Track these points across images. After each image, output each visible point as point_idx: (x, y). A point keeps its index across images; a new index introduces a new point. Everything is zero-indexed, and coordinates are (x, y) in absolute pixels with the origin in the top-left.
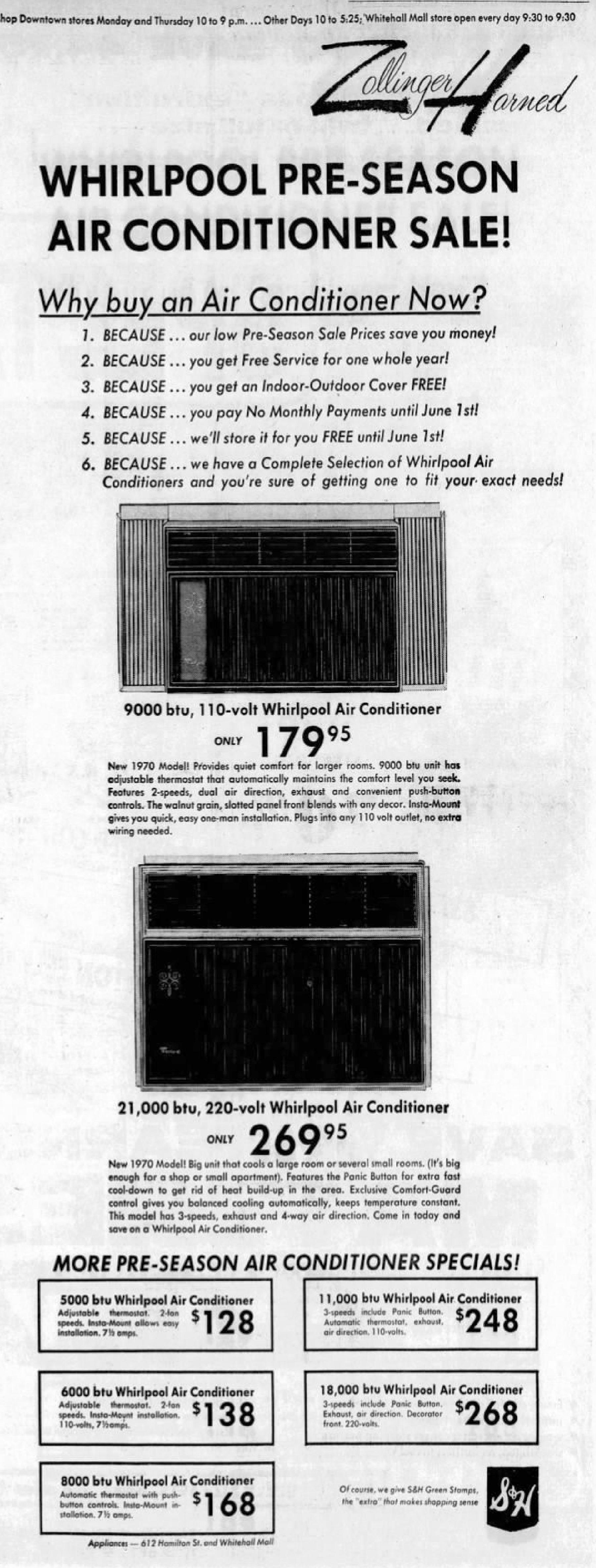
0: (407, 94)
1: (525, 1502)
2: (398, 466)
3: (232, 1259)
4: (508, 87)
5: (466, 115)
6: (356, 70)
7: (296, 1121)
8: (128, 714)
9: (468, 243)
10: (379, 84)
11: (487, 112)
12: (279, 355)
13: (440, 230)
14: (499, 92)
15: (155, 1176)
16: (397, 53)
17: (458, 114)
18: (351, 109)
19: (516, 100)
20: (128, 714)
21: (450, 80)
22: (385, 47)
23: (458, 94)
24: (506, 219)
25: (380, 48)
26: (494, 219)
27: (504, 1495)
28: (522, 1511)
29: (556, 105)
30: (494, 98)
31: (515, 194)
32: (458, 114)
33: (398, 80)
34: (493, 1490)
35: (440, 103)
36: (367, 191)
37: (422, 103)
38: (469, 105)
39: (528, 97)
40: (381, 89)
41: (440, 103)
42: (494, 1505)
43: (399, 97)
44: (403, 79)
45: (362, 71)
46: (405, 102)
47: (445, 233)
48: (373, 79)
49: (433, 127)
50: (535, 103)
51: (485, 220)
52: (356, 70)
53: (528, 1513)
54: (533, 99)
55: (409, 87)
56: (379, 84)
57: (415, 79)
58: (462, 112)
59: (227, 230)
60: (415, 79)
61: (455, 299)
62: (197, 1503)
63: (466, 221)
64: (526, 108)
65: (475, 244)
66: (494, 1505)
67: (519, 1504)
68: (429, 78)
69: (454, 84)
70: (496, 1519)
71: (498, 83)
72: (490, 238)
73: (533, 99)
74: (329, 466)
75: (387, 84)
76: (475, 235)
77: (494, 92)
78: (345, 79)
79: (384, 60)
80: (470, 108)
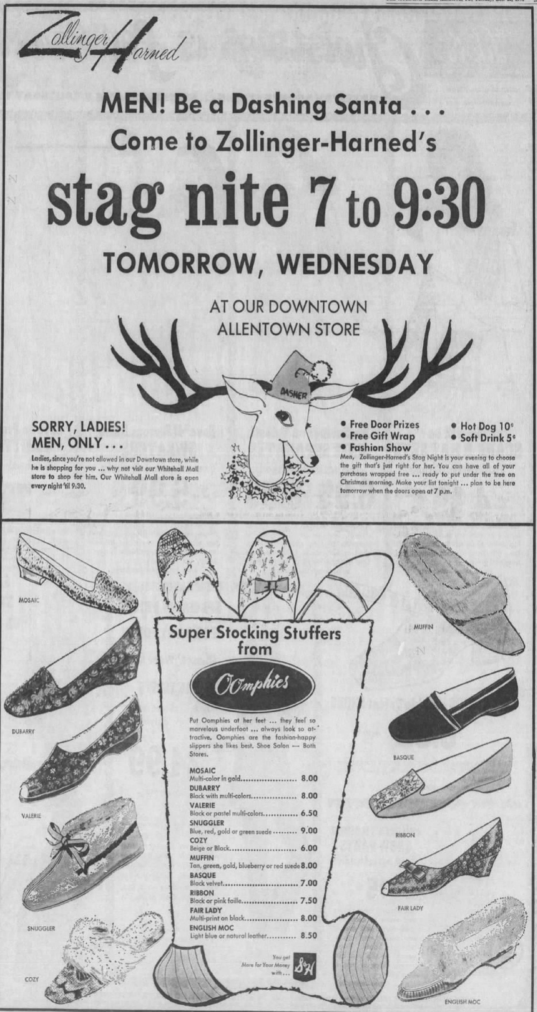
0: (79, 45)
1: (310, 969)
4: (142, 44)
5: (115, 61)
6: (48, 29)
10: (63, 39)
11: (129, 59)
14: (138, 47)
15: (271, 866)
16: (74, 19)
17: (111, 60)
18: (43, 54)
19: (148, 52)
21: (107, 38)
22: (67, 15)
23: (111, 47)
27: (301, 965)
28: (309, 972)
29: (173, 56)
30: (134, 51)
32: (111, 60)
34: (296, 964)
35: (101, 53)
37: (89, 53)
38: (118, 54)
39: (155, 51)
41: (101, 53)
43: (74, 47)
44: (78, 35)
45: (52, 30)
46: (78, 51)
48: (58, 36)
49: (95, 68)
50: (159, 55)
52: (48, 29)
53: (311, 974)
54: (159, 52)
55: (81, 42)
56: (63, 39)
57: (85, 36)
58: (113, 59)
59: (324, 262)
60: (85, 36)
64: (154, 57)
66: (296, 970)
67: (307, 970)
68: (93, 37)
69: (109, 41)
71: (136, 41)
73: (159, 52)
75: (67, 39)
77: (134, 46)
78: (40, 35)
79: (66, 23)
80: (119, 56)
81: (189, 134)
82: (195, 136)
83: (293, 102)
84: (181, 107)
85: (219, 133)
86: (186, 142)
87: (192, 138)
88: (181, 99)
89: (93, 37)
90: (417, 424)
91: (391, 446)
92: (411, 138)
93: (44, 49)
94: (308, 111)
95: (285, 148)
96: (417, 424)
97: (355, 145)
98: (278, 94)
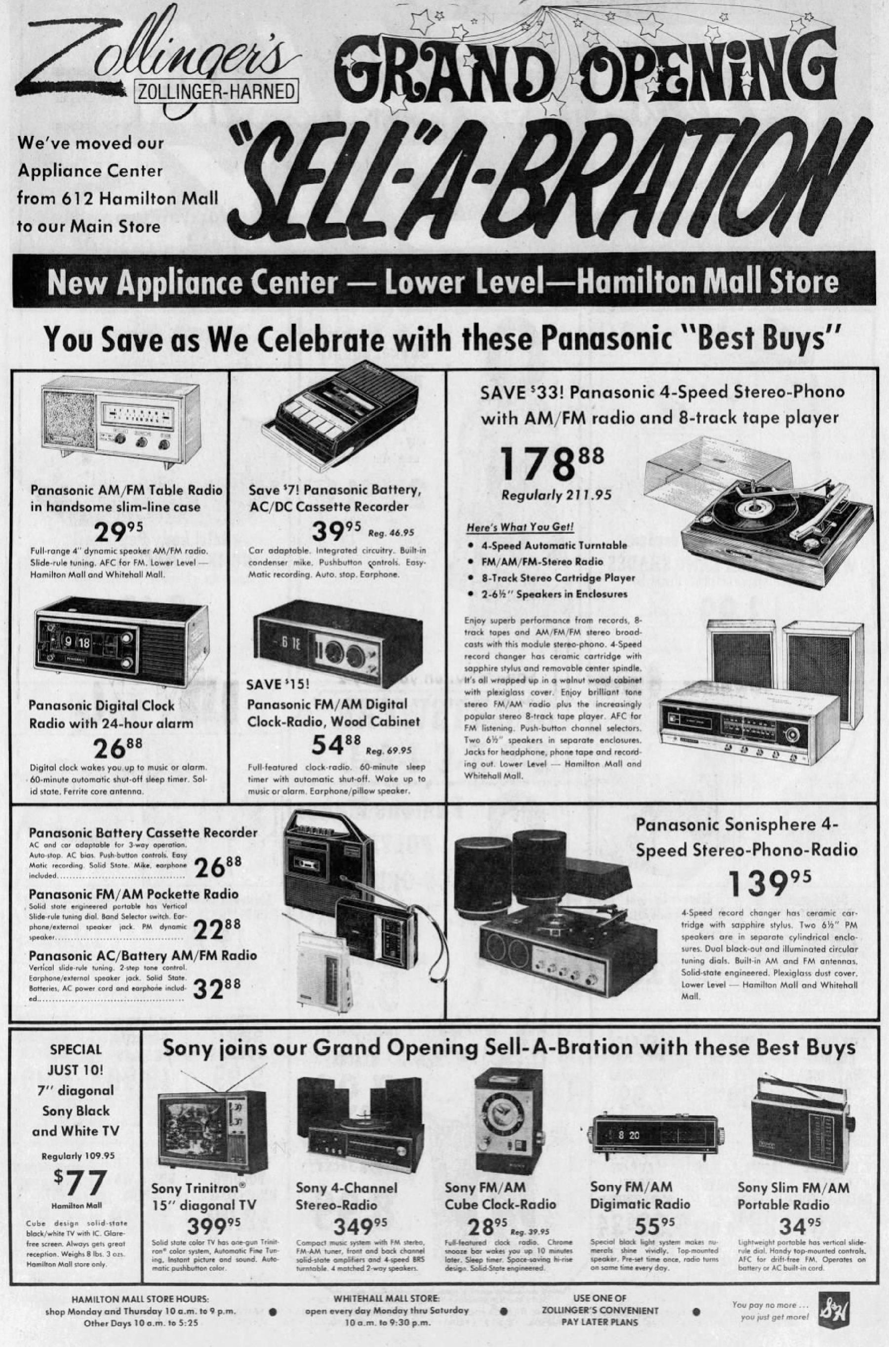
2: (75, 1073)
12: (111, 328)
22: (99, 26)
25: (93, 26)
27: (828, 1308)
33: (162, 52)
34: (822, 1305)
36: (680, 397)
40: (129, 68)
42: (823, 1312)
44: (171, 51)
46: (120, 84)
53: (843, 1319)
56: (128, 58)
61: (400, 338)
62: (58, 1181)
66: (822, 1315)
67: (838, 1313)
68: (218, 51)
74: (488, 1053)
75: (142, 59)
83: (100, 226)
84: (763, 1050)
86: (17, 227)
88: (762, 1043)
89: (218, 51)
93: (59, 83)
94: (461, 1053)
95: (468, 1052)
98: (781, 818)
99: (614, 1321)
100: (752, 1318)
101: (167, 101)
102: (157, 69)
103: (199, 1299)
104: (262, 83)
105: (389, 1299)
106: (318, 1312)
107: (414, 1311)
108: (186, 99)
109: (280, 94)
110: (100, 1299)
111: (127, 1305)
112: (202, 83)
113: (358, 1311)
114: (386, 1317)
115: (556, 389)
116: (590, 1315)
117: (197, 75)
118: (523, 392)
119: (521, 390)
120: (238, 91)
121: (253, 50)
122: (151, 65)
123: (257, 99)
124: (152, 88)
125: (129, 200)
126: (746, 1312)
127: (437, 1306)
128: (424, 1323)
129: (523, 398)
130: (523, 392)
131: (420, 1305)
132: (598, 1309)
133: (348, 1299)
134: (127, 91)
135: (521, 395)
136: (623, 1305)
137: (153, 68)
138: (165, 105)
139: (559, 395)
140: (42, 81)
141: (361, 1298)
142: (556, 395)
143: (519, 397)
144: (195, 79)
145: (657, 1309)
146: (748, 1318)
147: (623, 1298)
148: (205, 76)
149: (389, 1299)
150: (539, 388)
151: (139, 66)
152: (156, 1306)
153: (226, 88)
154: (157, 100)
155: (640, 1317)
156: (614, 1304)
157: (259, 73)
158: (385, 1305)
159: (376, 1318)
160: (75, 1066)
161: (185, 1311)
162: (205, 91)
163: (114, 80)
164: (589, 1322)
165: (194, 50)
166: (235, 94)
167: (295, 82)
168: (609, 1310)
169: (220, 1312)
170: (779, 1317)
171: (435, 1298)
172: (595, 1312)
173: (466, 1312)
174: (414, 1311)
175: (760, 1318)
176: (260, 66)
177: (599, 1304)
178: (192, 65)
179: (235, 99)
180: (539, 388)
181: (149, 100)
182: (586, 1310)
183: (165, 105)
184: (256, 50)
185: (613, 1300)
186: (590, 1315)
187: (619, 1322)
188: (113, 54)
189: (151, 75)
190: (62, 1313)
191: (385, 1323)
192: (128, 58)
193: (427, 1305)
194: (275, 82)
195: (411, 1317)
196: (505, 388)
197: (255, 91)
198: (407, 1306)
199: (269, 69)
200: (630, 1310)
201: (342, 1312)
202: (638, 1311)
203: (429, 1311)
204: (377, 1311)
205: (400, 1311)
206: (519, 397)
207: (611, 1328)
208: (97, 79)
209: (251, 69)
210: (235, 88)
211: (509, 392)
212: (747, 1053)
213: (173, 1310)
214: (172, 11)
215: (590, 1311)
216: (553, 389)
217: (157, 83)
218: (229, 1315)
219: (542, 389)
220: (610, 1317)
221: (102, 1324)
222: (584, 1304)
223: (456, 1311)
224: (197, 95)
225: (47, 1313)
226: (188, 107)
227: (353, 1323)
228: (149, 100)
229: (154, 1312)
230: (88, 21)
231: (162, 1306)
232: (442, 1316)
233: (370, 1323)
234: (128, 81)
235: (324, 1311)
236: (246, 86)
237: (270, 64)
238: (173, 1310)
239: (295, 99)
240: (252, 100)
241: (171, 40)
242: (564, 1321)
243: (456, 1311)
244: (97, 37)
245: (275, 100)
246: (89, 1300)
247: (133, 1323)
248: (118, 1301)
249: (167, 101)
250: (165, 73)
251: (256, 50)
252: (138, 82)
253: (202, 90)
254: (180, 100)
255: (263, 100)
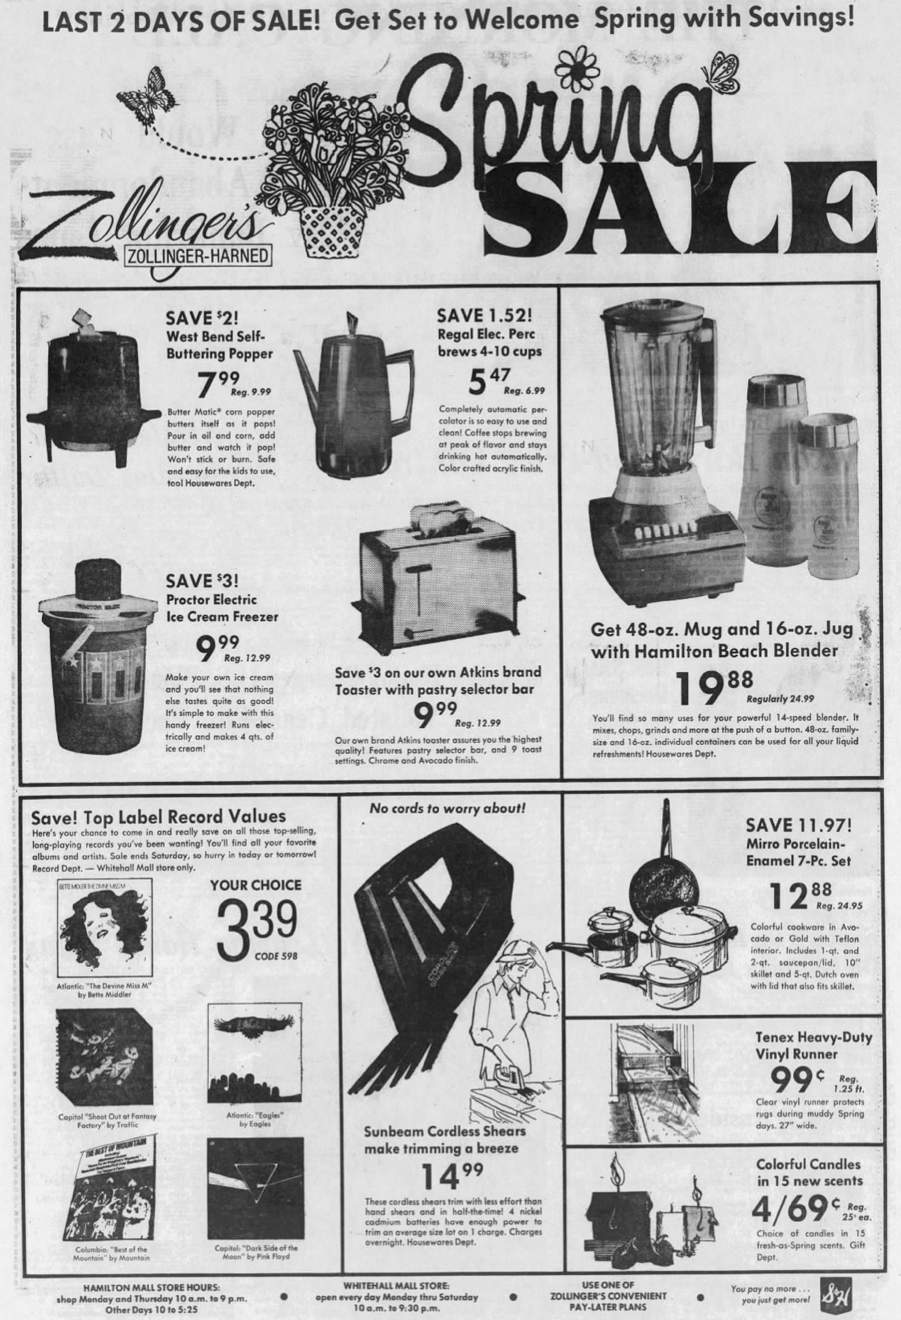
3: (374, 810)
7: (807, 1192)
8: (223, 384)
9: (292, 28)
13: (273, 19)
20: (223, 384)
22: (93, 197)
24: (317, 11)
25: (90, 198)
26: (309, 11)
27: (831, 1293)
28: (842, 1303)
31: (603, 85)
33: (150, 221)
34: (824, 1291)
40: (120, 234)
47: (277, 21)
51: (302, 12)
53: (846, 1304)
61: (473, 15)
63: (290, 12)
65: (295, 28)
66: (825, 1299)
67: (840, 1299)
70: (824, 1308)
72: (306, 24)
75: (131, 227)
76: (296, 22)
81: (438, 14)
82: (444, 16)
84: (724, 653)
85: (201, 375)
86: (435, 21)
87: (441, 18)
90: (860, 904)
91: (490, 1129)
92: (616, 29)
96: (860, 904)
97: (653, 654)
99: (622, 1306)
100: (754, 1301)
101: (154, 264)
102: (145, 236)
103: (209, 1287)
104: (239, 248)
105: (399, 1286)
106: (329, 1298)
107: (423, 1297)
108: (171, 263)
109: (255, 258)
110: (111, 1288)
111: (138, 1293)
112: (185, 248)
113: (368, 1298)
114: (396, 1303)
115: (230, 577)
116: (599, 1301)
117: (181, 241)
118: (210, 581)
119: (208, 578)
120: (218, 255)
121: (231, 219)
122: (139, 232)
123: (235, 263)
124: (141, 253)
125: (664, 653)
126: (745, 1296)
127: (446, 1293)
128: (433, 1308)
129: (210, 586)
130: (210, 581)
131: (429, 1292)
132: (606, 1295)
133: (358, 1286)
134: (118, 257)
135: (208, 584)
136: (630, 1291)
137: (142, 235)
138: (152, 268)
139: (233, 584)
140: (43, 246)
141: (370, 1286)
142: (230, 584)
143: (206, 586)
144: (179, 245)
145: (665, 1294)
146: (749, 1301)
147: (631, 1284)
148: (188, 242)
149: (399, 1286)
150: (225, 577)
151: (129, 233)
152: (166, 1294)
153: (207, 252)
154: (145, 263)
155: (649, 1303)
156: (621, 1290)
157: (236, 239)
158: (395, 1292)
159: (385, 1304)
160: (96, 15)
161: (195, 1299)
162: (188, 256)
163: (107, 245)
164: (599, 1307)
165: (178, 219)
166: (215, 258)
167: (268, 248)
168: (617, 1296)
169: (231, 1299)
170: (780, 1300)
171: (444, 1286)
172: (604, 1298)
173: (476, 1298)
174: (423, 1297)
175: (761, 1301)
176: (237, 233)
177: (607, 1291)
178: (176, 233)
179: (216, 263)
180: (225, 577)
181: (137, 264)
182: (595, 1296)
183: (152, 268)
184: (234, 219)
185: (621, 1286)
186: (599, 1301)
187: (628, 1307)
188: (106, 222)
189: (140, 241)
190: (73, 1301)
191: (394, 1309)
192: (119, 226)
193: (436, 1292)
194: (250, 247)
195: (420, 1303)
196: (191, 576)
197: (233, 256)
198: (417, 1293)
199: (244, 236)
200: (637, 1295)
201: (351, 1298)
202: (643, 1296)
203: (439, 1298)
204: (387, 1297)
205: (410, 1298)
206: (206, 586)
207: (619, 1312)
208: (91, 244)
209: (229, 236)
210: (215, 252)
211: (196, 580)
212: (576, 26)
213: (183, 1298)
214: (160, 182)
215: (600, 1297)
216: (227, 578)
217: (145, 248)
218: (239, 1303)
219: (227, 578)
220: (618, 1302)
221: (124, 1311)
222: (593, 1290)
223: (466, 1298)
224: (181, 259)
225: (58, 1301)
226: (174, 269)
227: (362, 1308)
228: (137, 264)
229: (165, 1299)
230: (83, 193)
231: (173, 1294)
232: (451, 1302)
233: (380, 1309)
234: (118, 245)
235: (334, 1297)
236: (225, 251)
237: (245, 231)
238: (183, 1298)
239: (268, 263)
240: (231, 264)
241: (158, 210)
242: (572, 1306)
243: (466, 1298)
244: (92, 206)
245: (250, 263)
246: (100, 1288)
247: (154, 1310)
248: (128, 1289)
249: (154, 264)
250: (153, 240)
251: (234, 219)
252: (128, 248)
253: (185, 254)
254: (166, 264)
255: (240, 264)
